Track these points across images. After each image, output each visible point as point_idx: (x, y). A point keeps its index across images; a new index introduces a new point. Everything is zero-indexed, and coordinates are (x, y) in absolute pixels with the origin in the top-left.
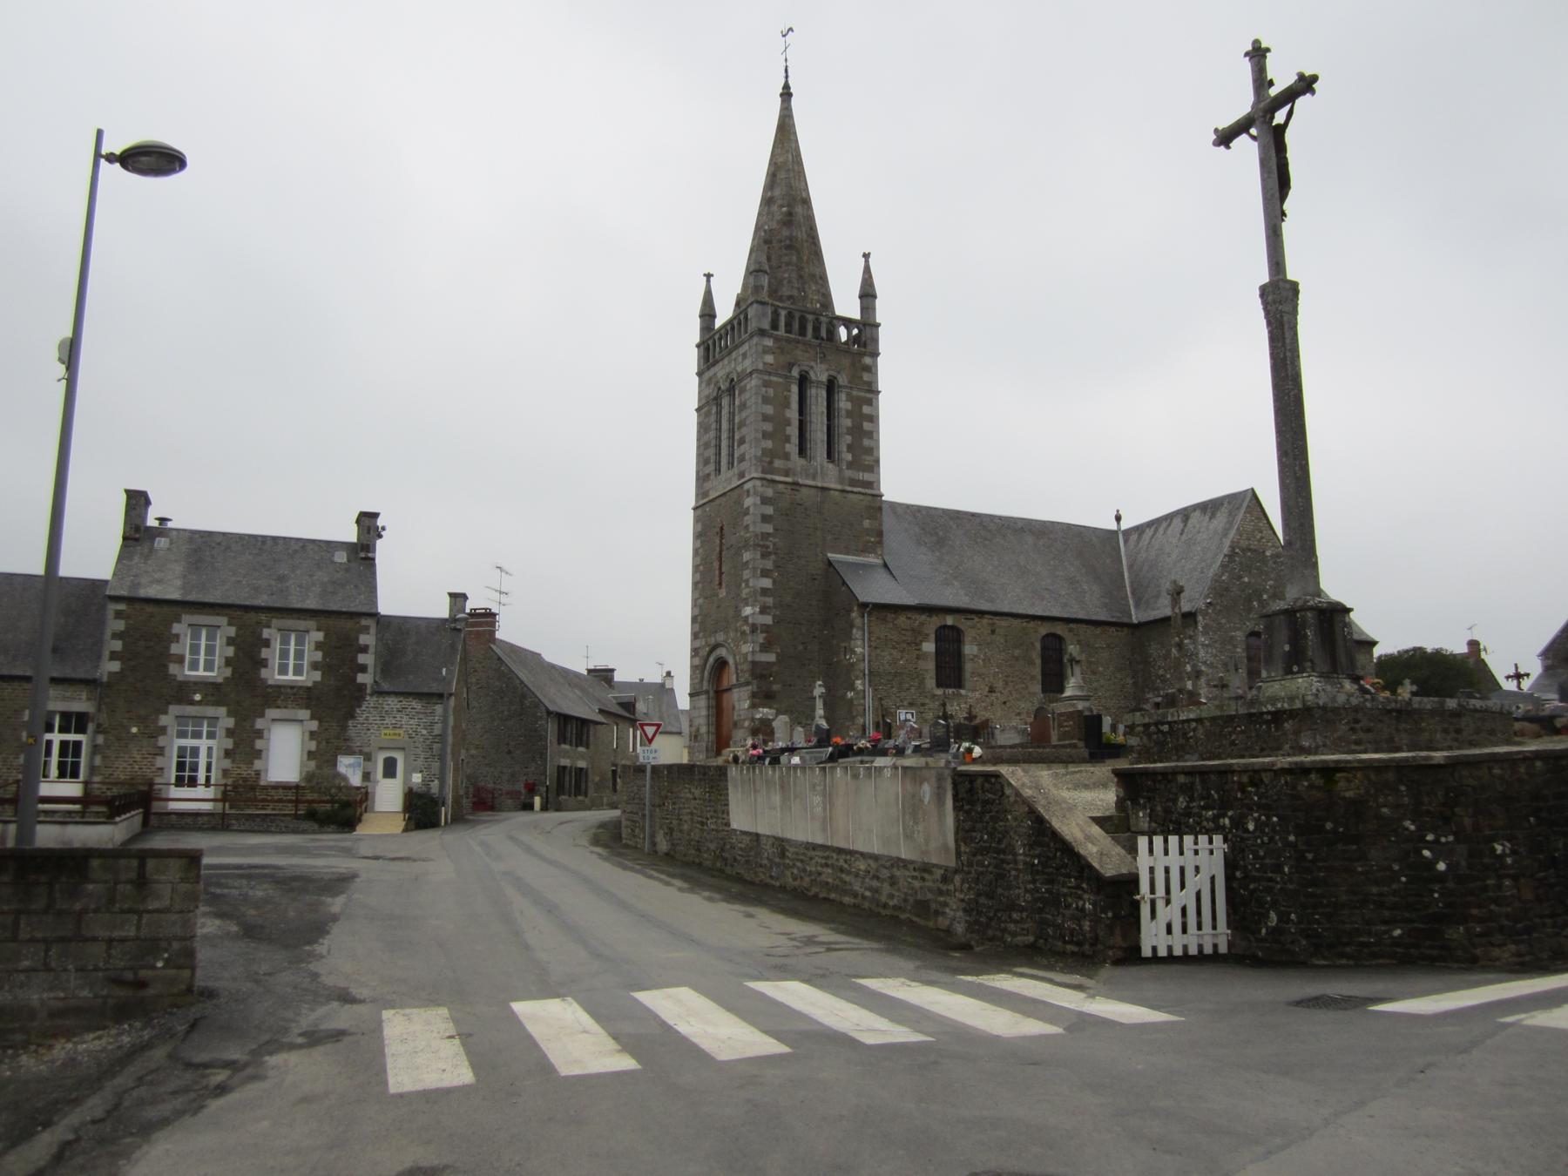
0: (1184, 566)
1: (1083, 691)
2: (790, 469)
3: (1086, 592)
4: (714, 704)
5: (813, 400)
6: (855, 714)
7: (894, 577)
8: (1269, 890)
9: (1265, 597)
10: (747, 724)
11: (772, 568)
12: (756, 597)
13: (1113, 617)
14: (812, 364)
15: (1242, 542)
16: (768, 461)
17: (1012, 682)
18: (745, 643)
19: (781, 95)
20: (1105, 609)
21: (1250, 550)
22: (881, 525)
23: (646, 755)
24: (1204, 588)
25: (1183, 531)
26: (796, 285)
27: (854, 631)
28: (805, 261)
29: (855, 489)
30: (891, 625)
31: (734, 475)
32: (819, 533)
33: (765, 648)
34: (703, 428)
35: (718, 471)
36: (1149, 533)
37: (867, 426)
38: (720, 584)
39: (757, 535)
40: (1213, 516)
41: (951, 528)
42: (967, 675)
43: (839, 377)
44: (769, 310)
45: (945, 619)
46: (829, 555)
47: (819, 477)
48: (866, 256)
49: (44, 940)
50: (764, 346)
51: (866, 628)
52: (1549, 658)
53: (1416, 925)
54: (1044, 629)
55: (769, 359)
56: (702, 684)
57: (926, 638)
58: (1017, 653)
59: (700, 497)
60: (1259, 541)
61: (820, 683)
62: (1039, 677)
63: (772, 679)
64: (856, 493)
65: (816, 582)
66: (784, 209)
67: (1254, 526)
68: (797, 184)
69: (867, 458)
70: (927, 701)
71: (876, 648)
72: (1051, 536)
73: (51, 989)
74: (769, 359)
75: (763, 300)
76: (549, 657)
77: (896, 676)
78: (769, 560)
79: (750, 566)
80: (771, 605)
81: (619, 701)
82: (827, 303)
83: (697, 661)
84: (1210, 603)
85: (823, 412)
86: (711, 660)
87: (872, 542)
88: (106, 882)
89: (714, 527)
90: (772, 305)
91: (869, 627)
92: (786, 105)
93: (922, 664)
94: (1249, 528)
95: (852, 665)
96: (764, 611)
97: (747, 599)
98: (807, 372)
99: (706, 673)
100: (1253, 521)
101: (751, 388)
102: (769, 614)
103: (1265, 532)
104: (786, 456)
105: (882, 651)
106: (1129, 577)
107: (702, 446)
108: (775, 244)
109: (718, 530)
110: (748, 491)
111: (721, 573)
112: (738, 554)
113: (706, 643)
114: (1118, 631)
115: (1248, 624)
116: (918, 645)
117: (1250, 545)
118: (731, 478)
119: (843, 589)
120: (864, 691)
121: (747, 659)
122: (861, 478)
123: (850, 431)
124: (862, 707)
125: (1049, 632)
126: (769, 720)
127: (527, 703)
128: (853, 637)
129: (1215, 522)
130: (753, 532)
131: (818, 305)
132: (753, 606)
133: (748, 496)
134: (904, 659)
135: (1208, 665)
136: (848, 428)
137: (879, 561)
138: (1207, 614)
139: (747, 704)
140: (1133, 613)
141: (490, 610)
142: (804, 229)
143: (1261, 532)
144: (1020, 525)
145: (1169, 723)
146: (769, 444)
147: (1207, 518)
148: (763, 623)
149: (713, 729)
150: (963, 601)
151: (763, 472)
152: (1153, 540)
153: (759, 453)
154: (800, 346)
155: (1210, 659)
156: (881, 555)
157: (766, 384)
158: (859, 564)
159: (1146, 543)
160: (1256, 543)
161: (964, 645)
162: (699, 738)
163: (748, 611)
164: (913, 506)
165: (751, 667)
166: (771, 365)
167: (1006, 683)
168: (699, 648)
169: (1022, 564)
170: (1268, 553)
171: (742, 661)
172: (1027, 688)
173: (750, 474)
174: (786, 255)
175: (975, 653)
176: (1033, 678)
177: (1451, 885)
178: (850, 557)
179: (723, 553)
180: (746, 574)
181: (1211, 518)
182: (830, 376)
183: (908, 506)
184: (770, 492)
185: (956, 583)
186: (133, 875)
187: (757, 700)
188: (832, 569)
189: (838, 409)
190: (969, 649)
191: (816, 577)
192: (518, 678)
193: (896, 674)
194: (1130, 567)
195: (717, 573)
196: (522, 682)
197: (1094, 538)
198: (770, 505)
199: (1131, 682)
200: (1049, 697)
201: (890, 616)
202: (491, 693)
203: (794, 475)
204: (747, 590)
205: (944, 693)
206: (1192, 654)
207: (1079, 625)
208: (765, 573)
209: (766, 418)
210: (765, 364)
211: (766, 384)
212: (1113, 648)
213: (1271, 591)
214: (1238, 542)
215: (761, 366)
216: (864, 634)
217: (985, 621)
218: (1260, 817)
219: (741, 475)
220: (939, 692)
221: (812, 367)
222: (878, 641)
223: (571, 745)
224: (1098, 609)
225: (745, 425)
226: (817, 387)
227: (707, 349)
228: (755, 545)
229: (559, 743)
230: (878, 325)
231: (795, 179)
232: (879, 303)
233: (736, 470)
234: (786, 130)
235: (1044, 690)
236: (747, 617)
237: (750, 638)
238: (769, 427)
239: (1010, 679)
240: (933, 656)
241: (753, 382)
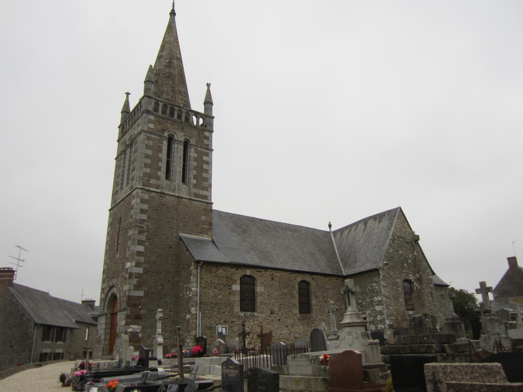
0: (368, 246)
1: (359, 318)
2: (160, 185)
3: (319, 260)
4: (110, 322)
5: (176, 150)
6: (190, 328)
7: (217, 247)
11: (145, 240)
12: (133, 256)
13: (334, 272)
14: (176, 131)
16: (147, 179)
17: (283, 307)
18: (125, 284)
19: (170, 14)
20: (329, 268)
21: (401, 237)
22: (211, 219)
24: (382, 256)
25: (364, 230)
26: (170, 94)
27: (192, 277)
28: (176, 84)
30: (214, 274)
31: (129, 188)
32: (175, 221)
33: (137, 287)
34: (117, 167)
35: (122, 188)
36: (346, 232)
37: (205, 166)
38: (117, 250)
39: (137, 220)
40: (380, 221)
41: (250, 225)
42: (258, 304)
43: (191, 140)
44: (153, 102)
45: (246, 272)
46: (180, 234)
47: (177, 191)
48: (208, 85)
50: (149, 119)
51: (199, 275)
52: (496, 294)
54: (300, 278)
55: (152, 126)
56: (104, 310)
57: (234, 282)
58: (285, 291)
59: (113, 203)
60: (405, 233)
61: (160, 310)
62: (298, 305)
63: (140, 306)
64: (197, 201)
65: (172, 249)
66: (167, 60)
67: (402, 225)
68: (175, 50)
69: (205, 183)
70: (235, 320)
71: (204, 288)
72: (300, 232)
74: (152, 126)
75: (150, 96)
76: (53, 294)
77: (216, 305)
78: (143, 235)
79: (132, 239)
80: (143, 262)
81: (93, 316)
82: (187, 103)
83: (103, 296)
84: (385, 264)
85: (181, 157)
86: (109, 295)
87: (206, 228)
89: (117, 219)
90: (155, 99)
91: (201, 275)
92: (172, 19)
93: (232, 298)
94: (400, 226)
95: (190, 298)
96: (137, 265)
97: (128, 258)
98: (173, 136)
99: (106, 303)
100: (401, 223)
102: (141, 267)
103: (407, 229)
104: (158, 178)
105: (208, 290)
106: (339, 253)
107: (117, 176)
108: (161, 76)
109: (119, 220)
111: (118, 244)
112: (127, 232)
113: (108, 285)
114: (336, 279)
115: (403, 275)
116: (230, 286)
117: (401, 234)
118: (127, 191)
119: (187, 253)
120: (196, 314)
121: (126, 294)
122: (201, 193)
123: (196, 168)
124: (195, 324)
125: (302, 280)
126: (137, 332)
127: (24, 319)
128: (191, 281)
129: (382, 224)
130: (135, 218)
132: (131, 262)
133: (134, 198)
134: (222, 295)
135: (386, 297)
136: (195, 166)
137: (210, 239)
138: (384, 269)
139: (123, 323)
140: (343, 269)
141: (12, 269)
142: (177, 70)
144: (284, 227)
146: (148, 170)
147: (377, 222)
148: (137, 272)
149: (108, 337)
150: (256, 261)
151: (143, 185)
152: (349, 235)
153: (142, 175)
154: (170, 121)
155: (387, 294)
156: (211, 236)
158: (197, 240)
159: (346, 236)
160: (403, 234)
161: (256, 286)
163: (128, 265)
164: (230, 213)
165: (127, 299)
166: (152, 129)
169: (287, 244)
171: (123, 295)
172: (291, 311)
174: (166, 80)
175: (263, 292)
176: (294, 305)
178: (193, 236)
179: (120, 232)
181: (379, 223)
182: (185, 139)
183: (227, 213)
184: (146, 197)
185: (252, 252)
187: (130, 320)
188: (181, 242)
189: (190, 156)
190: (259, 289)
191: (172, 246)
192: (21, 305)
193: (216, 304)
194: (338, 248)
195: (116, 244)
196: (23, 307)
197: (320, 235)
198: (146, 204)
199: (344, 307)
200: (303, 316)
201: (214, 269)
202: (6, 313)
203: (162, 188)
204: (129, 252)
205: (245, 314)
206: (377, 292)
207: (317, 276)
208: (140, 243)
209: (147, 156)
210: (148, 128)
211: (148, 139)
212: (335, 289)
214: (396, 233)
215: (146, 129)
216: (198, 278)
217: (268, 273)
219: (132, 188)
220: (242, 314)
221: (176, 133)
222: (206, 283)
223: (52, 340)
224: (326, 268)
225: (136, 160)
226: (178, 144)
227: (123, 128)
228: (134, 226)
229: (43, 340)
230: (213, 118)
231: (174, 48)
232: (214, 107)
233: (129, 186)
234: (171, 28)
235: (300, 313)
237: (128, 281)
238: (148, 161)
239: (282, 306)
240: (239, 293)
241: (142, 136)
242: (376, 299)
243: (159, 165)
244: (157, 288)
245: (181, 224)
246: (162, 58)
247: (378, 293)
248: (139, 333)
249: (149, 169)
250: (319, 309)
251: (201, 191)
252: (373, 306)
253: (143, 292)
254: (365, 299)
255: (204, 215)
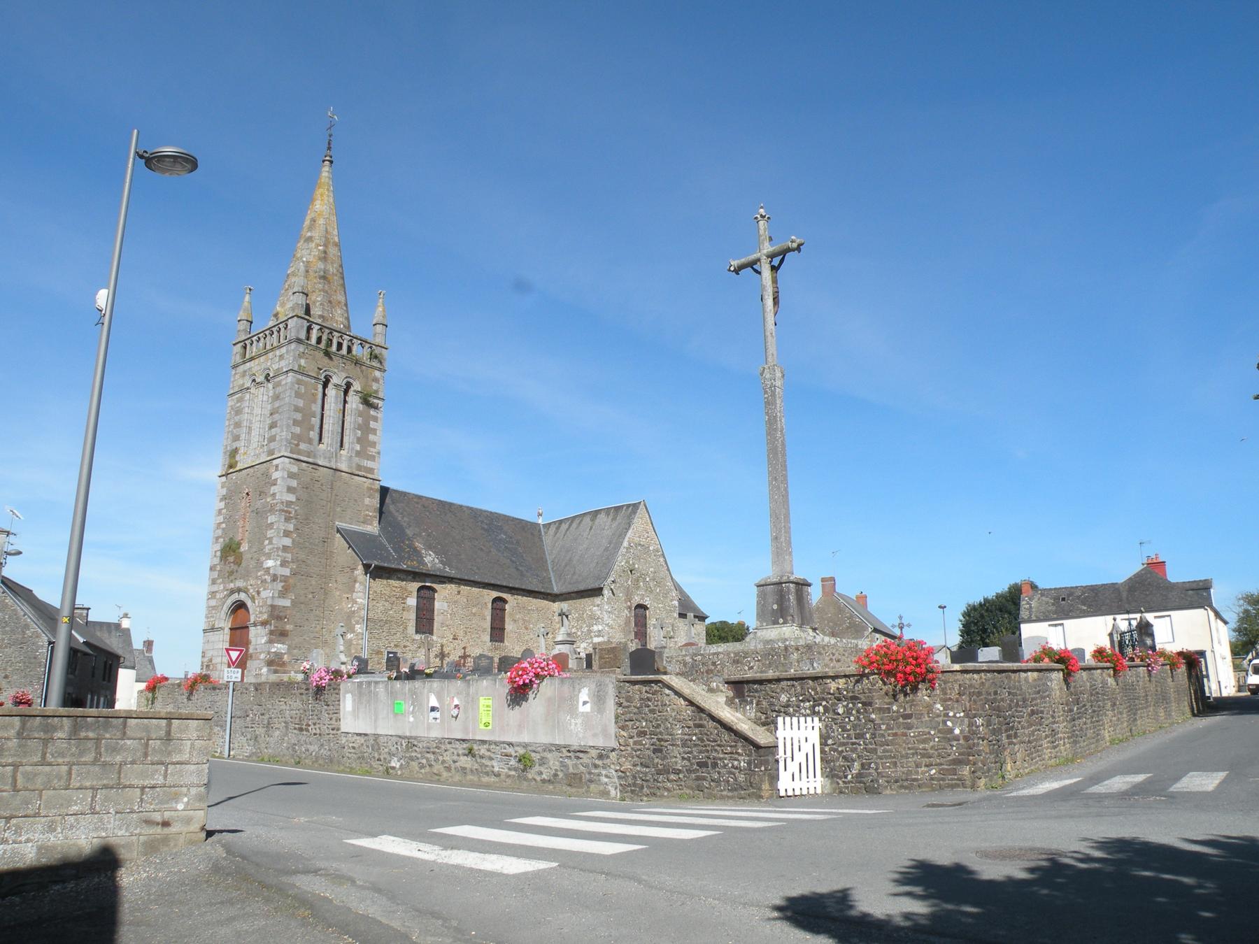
8: (854, 750)
9: (648, 579)
10: (262, 656)
15: (635, 539)
23: (229, 675)
27: (357, 585)
29: (360, 473)
33: (283, 594)
36: (564, 527)
39: (283, 502)
49: (92, 788)
53: (943, 766)
63: (286, 620)
66: (321, 248)
70: (408, 644)
73: (96, 829)
77: (387, 623)
87: (371, 516)
88: (140, 739)
96: (284, 564)
101: (286, 384)
110: (277, 466)
122: (365, 465)
126: (282, 653)
131: (342, 326)
133: (276, 470)
143: (648, 533)
145: (701, 655)
146: (297, 430)
153: (289, 437)
157: (299, 382)
162: (211, 667)
163: (270, 563)
167: (466, 633)
168: (216, 592)
170: (651, 548)
173: (280, 452)
176: (484, 630)
177: (961, 742)
180: (270, 533)
181: (612, 520)
184: (294, 469)
186: (162, 733)
190: (438, 605)
203: (315, 457)
205: (421, 637)
208: (287, 534)
209: (297, 409)
211: (299, 382)
213: (651, 575)
218: (848, 704)
220: (418, 637)
236: (269, 568)
238: (299, 416)
239: (469, 630)
242: (595, 628)
243: (312, 423)
244: (306, 597)
245: (338, 509)
246: (312, 241)
247: (597, 620)
248: (285, 654)
249: (299, 428)
250: (516, 637)
251: (366, 461)
252: (591, 637)
253: (290, 600)
254: (582, 627)
255: (369, 497)
